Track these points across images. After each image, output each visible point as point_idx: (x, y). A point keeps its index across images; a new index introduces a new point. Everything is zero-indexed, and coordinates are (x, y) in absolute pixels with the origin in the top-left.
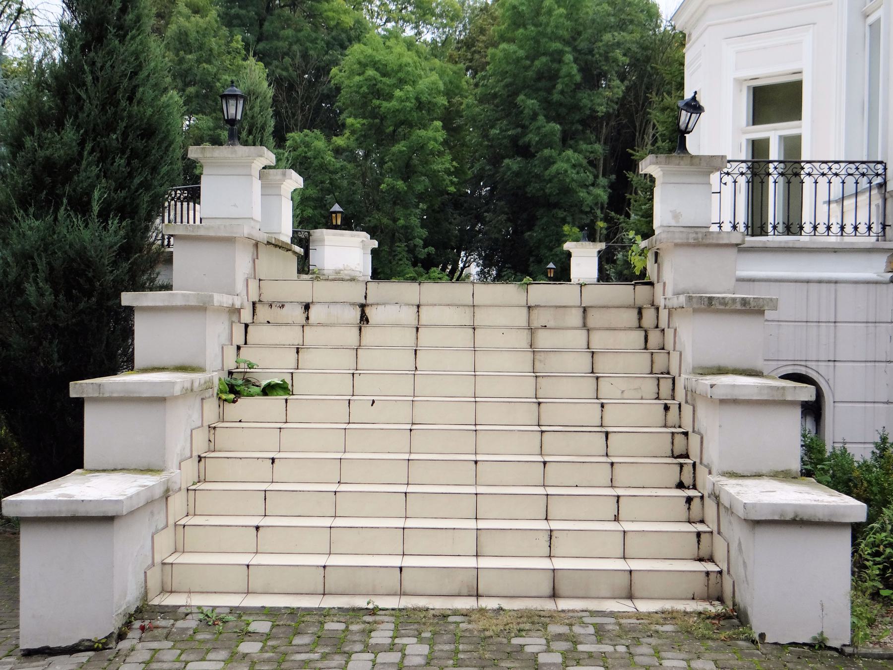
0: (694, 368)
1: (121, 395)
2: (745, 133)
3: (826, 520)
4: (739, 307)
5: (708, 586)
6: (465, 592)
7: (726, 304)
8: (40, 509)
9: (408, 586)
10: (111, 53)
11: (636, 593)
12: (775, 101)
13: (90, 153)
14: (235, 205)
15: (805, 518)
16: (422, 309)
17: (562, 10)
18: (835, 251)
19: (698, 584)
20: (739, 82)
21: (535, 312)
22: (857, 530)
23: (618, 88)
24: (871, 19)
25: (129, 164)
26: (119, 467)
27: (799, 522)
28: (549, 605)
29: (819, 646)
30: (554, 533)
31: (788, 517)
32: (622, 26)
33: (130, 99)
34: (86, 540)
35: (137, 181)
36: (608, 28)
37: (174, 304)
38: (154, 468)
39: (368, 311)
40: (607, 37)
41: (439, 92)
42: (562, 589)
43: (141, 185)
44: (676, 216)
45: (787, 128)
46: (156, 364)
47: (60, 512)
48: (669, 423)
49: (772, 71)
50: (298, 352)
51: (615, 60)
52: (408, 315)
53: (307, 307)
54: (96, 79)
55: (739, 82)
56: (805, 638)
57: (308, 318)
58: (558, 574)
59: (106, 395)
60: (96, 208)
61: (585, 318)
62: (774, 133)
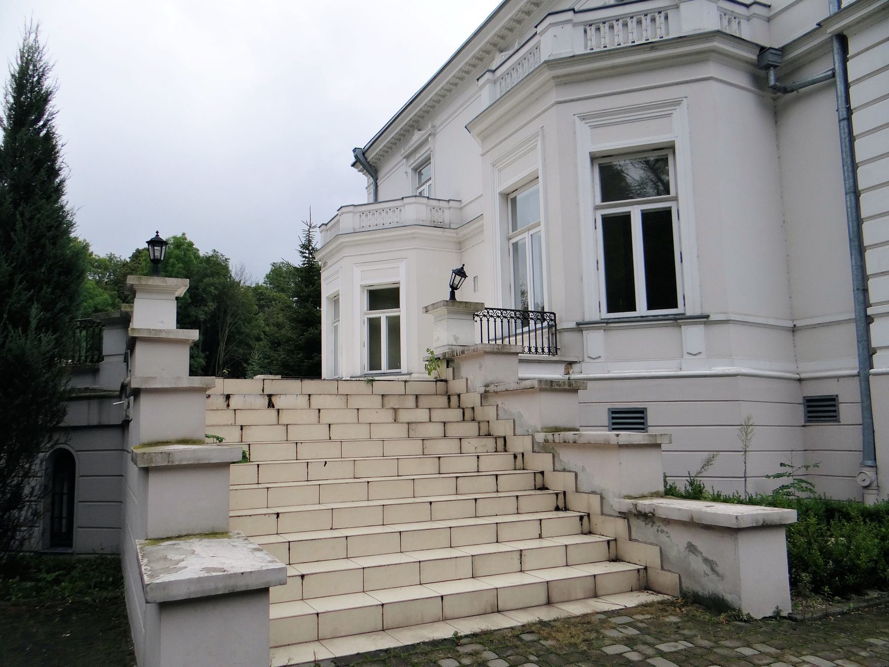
0: (542, 428)
1: (191, 462)
2: (366, 314)
3: (778, 523)
4: (567, 387)
5: (639, 580)
6: (489, 610)
7: (560, 386)
8: (193, 588)
9: (448, 612)
10: (38, 210)
11: (599, 593)
12: (384, 298)
13: (20, 283)
14: (162, 322)
15: (769, 523)
16: (312, 398)
17: (181, 265)
18: (539, 362)
19: (633, 579)
20: (363, 287)
21: (386, 399)
22: (791, 531)
23: (212, 306)
24: (514, 240)
25: (52, 293)
26: (184, 533)
27: (765, 526)
28: (546, 615)
29: (777, 616)
30: (523, 553)
31: (760, 523)
32: (212, 275)
33: (54, 244)
34: (238, 616)
35: (59, 306)
36: (206, 275)
37: (180, 386)
38: (218, 531)
39: (273, 399)
40: (206, 280)
41: (108, 305)
42: (555, 597)
43: (61, 310)
44: (456, 339)
45: (392, 312)
46: (160, 439)
47: (216, 589)
48: (517, 467)
49: (382, 280)
50: (242, 429)
51: (210, 292)
52: (302, 401)
53: (228, 397)
54: (24, 227)
55: (363, 287)
56: (769, 614)
57: (228, 405)
58: (551, 585)
59: (177, 463)
60: (34, 323)
61: (417, 402)
62: (383, 315)
